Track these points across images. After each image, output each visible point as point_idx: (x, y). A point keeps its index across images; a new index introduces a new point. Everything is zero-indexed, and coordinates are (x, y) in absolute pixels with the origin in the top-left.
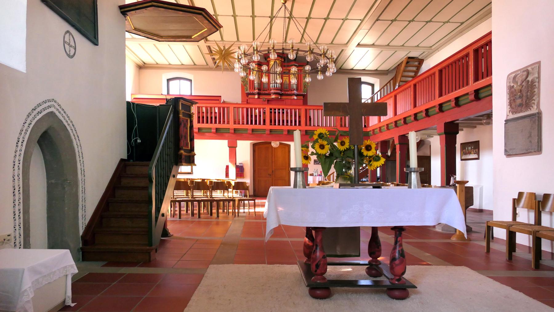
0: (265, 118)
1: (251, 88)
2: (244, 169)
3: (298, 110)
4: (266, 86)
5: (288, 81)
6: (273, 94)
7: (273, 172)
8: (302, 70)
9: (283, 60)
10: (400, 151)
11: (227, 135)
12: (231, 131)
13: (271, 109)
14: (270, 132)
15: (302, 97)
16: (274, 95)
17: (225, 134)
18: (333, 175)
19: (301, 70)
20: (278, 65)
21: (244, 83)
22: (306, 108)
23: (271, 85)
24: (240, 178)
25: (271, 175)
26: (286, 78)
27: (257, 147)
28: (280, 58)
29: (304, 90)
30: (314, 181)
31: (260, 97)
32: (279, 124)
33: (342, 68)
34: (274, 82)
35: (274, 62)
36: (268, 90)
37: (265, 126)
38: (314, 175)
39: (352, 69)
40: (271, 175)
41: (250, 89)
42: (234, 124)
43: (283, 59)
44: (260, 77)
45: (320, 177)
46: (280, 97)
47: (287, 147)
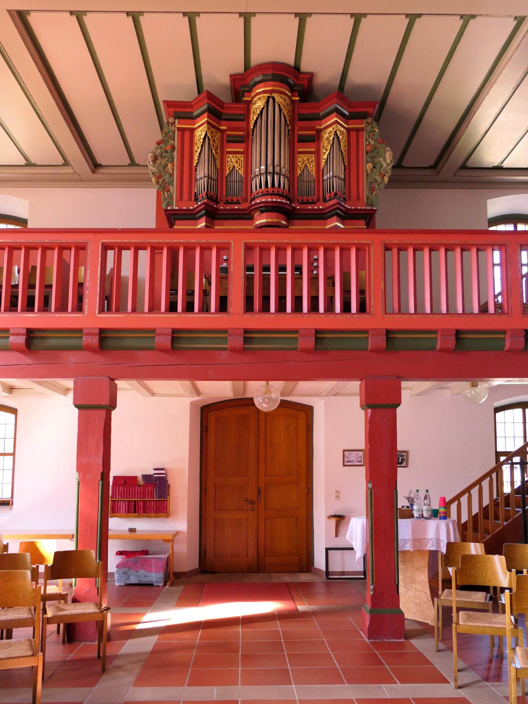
0: (226, 289)
1: (185, 197)
2: (169, 486)
3: (358, 250)
4: (236, 186)
5: (312, 167)
6: (262, 212)
7: (259, 492)
8: (362, 129)
9: (298, 98)
10: (109, 481)
11: (72, 358)
12: (86, 340)
13: (249, 248)
14: (247, 340)
15: (363, 222)
16: (265, 214)
17: (66, 353)
18: (456, 503)
19: (358, 130)
20: (280, 110)
21: (161, 181)
22: (387, 242)
23: (255, 183)
24: (157, 517)
25: (253, 503)
26: (305, 157)
27: (212, 416)
28: (285, 85)
29: (368, 198)
30: (417, 540)
31: (213, 224)
32: (281, 307)
33: (469, 164)
34: (263, 167)
35: (268, 102)
36: (245, 200)
37: (224, 315)
38: (416, 514)
39: (499, 168)
40: (253, 503)
41: (181, 199)
42: (101, 311)
43: (297, 93)
44: (218, 157)
45: (443, 524)
46: (284, 222)
47: (302, 415)
